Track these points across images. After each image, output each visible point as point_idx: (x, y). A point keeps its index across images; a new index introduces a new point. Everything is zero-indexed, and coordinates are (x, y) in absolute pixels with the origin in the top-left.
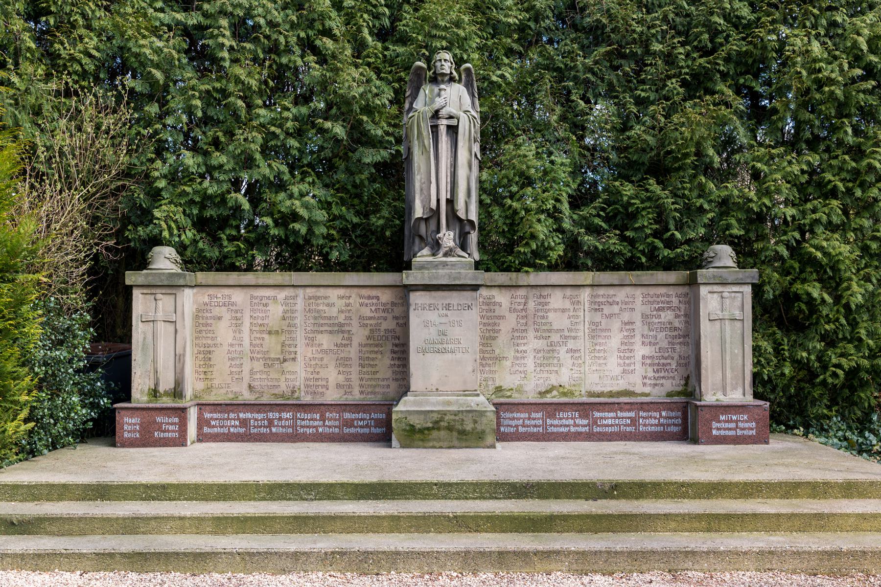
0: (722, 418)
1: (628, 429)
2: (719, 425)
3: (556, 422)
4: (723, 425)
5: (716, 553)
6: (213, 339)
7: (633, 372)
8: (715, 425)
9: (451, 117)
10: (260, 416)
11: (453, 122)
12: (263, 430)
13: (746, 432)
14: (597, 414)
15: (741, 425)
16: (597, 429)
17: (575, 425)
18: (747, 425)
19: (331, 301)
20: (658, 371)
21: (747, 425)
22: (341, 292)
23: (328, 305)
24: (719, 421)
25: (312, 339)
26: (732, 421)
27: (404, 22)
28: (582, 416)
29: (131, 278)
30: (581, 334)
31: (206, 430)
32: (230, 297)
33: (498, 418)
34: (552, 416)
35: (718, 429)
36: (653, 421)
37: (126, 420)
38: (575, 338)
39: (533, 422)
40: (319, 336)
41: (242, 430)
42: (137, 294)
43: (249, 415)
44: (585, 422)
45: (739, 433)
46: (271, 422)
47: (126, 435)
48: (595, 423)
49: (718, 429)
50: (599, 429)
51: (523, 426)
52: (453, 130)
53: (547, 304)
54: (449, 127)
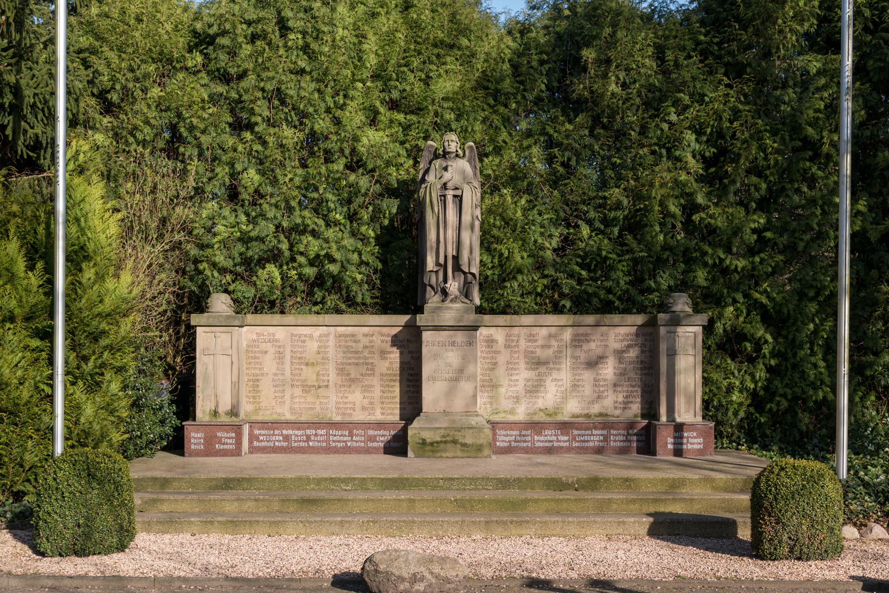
3: (542, 438)
10: (299, 433)
11: (458, 193)
12: (302, 444)
14: (576, 432)
17: (558, 441)
21: (695, 441)
23: (355, 341)
29: (195, 319)
31: (256, 444)
37: (193, 434)
40: (348, 367)
42: (198, 329)
44: (566, 438)
47: (193, 447)
48: (574, 439)
49: (334, 441)
51: (515, 441)
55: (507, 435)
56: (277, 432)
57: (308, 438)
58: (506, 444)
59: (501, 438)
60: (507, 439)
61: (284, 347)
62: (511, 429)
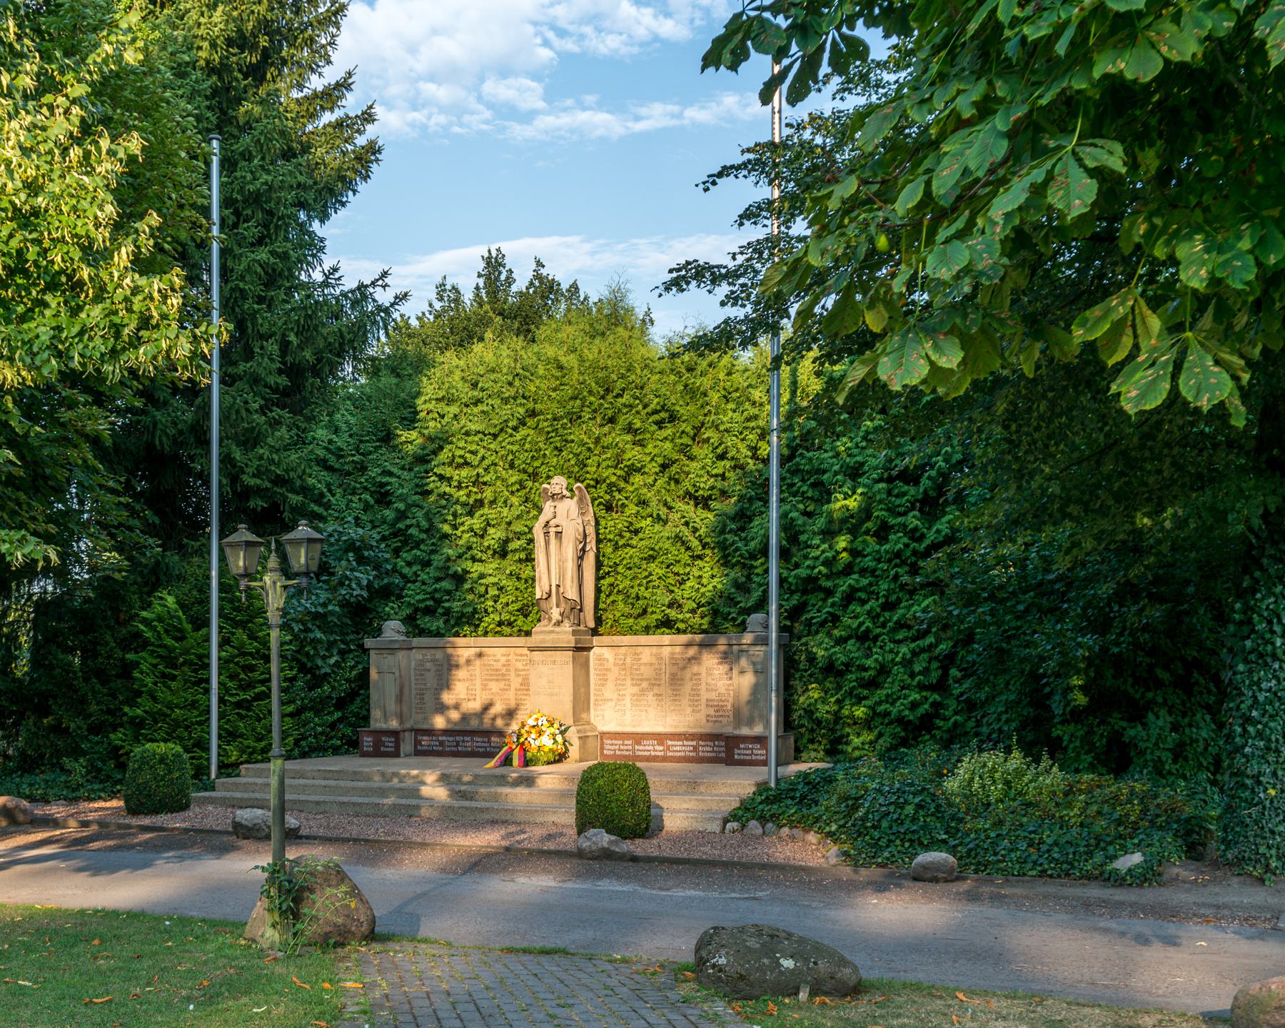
8: (736, 751)
10: (451, 739)
11: (559, 529)
14: (670, 743)
16: (670, 754)
27: (1066, 738)
28: (660, 744)
34: (639, 743)
54: (557, 533)
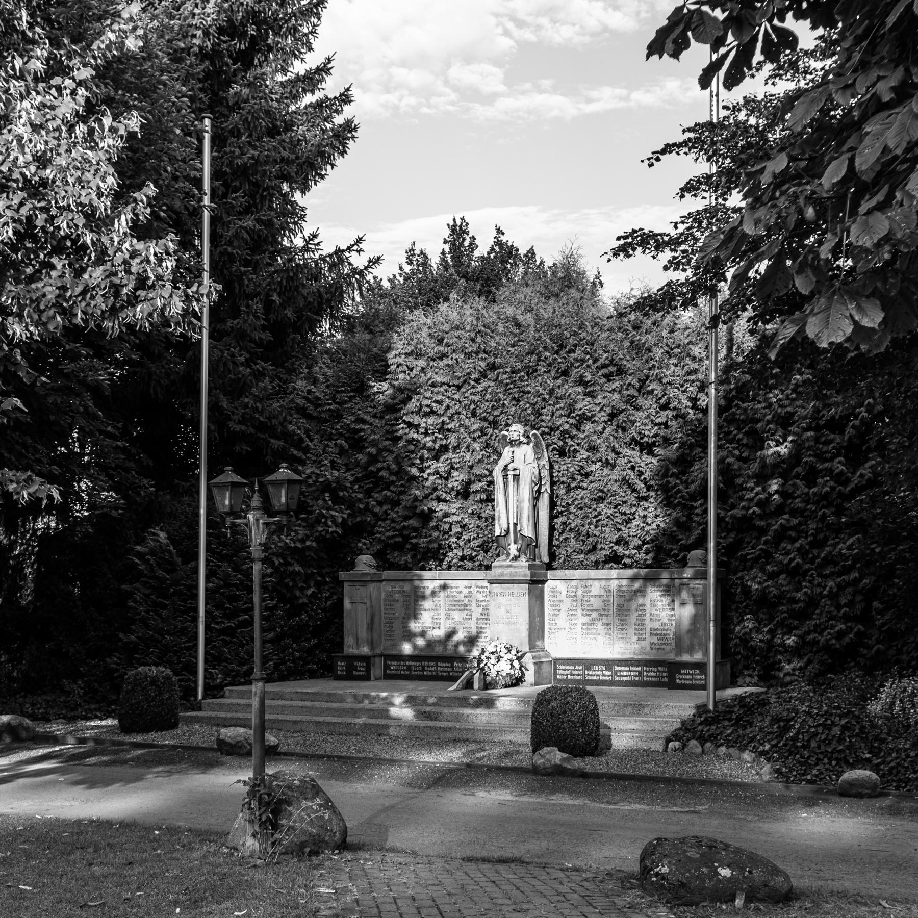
0: (683, 672)
1: (637, 679)
2: (681, 677)
3: (591, 673)
4: (684, 677)
5: (584, 775)
6: (394, 614)
7: (644, 639)
8: (678, 676)
9: (515, 469)
10: (418, 664)
11: (517, 472)
12: (419, 673)
13: (698, 682)
14: (617, 668)
15: (695, 677)
17: (603, 675)
18: (699, 677)
19: (459, 590)
20: (660, 639)
21: (699, 677)
22: (466, 583)
23: (458, 592)
24: (681, 674)
25: (449, 615)
26: (689, 674)
29: (343, 575)
30: (611, 612)
31: (388, 672)
32: (403, 587)
33: (555, 669)
35: (680, 679)
36: (653, 674)
37: (339, 663)
38: (607, 615)
39: (577, 673)
40: (453, 613)
41: (408, 673)
42: (346, 584)
43: (411, 663)
44: (609, 673)
45: (694, 682)
46: (423, 669)
47: (339, 673)
48: (615, 674)
49: (680, 679)
50: (618, 678)
51: (571, 675)
52: (516, 478)
53: (590, 592)
54: (514, 476)
55: (564, 670)
56: (402, 663)
57: (423, 669)
58: (564, 677)
59: (561, 672)
60: (565, 672)
61: (409, 596)
62: (568, 665)
